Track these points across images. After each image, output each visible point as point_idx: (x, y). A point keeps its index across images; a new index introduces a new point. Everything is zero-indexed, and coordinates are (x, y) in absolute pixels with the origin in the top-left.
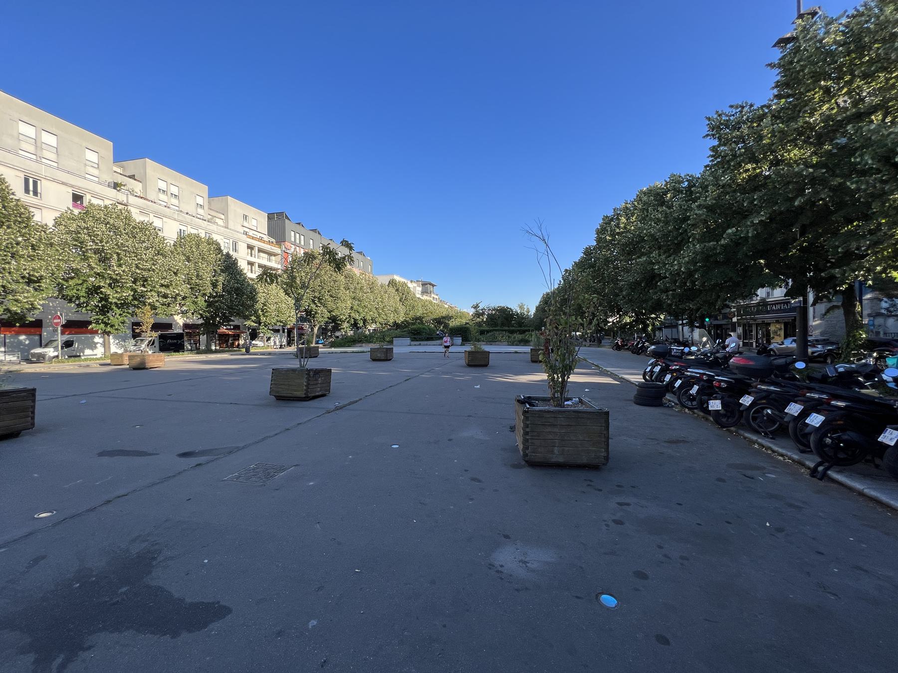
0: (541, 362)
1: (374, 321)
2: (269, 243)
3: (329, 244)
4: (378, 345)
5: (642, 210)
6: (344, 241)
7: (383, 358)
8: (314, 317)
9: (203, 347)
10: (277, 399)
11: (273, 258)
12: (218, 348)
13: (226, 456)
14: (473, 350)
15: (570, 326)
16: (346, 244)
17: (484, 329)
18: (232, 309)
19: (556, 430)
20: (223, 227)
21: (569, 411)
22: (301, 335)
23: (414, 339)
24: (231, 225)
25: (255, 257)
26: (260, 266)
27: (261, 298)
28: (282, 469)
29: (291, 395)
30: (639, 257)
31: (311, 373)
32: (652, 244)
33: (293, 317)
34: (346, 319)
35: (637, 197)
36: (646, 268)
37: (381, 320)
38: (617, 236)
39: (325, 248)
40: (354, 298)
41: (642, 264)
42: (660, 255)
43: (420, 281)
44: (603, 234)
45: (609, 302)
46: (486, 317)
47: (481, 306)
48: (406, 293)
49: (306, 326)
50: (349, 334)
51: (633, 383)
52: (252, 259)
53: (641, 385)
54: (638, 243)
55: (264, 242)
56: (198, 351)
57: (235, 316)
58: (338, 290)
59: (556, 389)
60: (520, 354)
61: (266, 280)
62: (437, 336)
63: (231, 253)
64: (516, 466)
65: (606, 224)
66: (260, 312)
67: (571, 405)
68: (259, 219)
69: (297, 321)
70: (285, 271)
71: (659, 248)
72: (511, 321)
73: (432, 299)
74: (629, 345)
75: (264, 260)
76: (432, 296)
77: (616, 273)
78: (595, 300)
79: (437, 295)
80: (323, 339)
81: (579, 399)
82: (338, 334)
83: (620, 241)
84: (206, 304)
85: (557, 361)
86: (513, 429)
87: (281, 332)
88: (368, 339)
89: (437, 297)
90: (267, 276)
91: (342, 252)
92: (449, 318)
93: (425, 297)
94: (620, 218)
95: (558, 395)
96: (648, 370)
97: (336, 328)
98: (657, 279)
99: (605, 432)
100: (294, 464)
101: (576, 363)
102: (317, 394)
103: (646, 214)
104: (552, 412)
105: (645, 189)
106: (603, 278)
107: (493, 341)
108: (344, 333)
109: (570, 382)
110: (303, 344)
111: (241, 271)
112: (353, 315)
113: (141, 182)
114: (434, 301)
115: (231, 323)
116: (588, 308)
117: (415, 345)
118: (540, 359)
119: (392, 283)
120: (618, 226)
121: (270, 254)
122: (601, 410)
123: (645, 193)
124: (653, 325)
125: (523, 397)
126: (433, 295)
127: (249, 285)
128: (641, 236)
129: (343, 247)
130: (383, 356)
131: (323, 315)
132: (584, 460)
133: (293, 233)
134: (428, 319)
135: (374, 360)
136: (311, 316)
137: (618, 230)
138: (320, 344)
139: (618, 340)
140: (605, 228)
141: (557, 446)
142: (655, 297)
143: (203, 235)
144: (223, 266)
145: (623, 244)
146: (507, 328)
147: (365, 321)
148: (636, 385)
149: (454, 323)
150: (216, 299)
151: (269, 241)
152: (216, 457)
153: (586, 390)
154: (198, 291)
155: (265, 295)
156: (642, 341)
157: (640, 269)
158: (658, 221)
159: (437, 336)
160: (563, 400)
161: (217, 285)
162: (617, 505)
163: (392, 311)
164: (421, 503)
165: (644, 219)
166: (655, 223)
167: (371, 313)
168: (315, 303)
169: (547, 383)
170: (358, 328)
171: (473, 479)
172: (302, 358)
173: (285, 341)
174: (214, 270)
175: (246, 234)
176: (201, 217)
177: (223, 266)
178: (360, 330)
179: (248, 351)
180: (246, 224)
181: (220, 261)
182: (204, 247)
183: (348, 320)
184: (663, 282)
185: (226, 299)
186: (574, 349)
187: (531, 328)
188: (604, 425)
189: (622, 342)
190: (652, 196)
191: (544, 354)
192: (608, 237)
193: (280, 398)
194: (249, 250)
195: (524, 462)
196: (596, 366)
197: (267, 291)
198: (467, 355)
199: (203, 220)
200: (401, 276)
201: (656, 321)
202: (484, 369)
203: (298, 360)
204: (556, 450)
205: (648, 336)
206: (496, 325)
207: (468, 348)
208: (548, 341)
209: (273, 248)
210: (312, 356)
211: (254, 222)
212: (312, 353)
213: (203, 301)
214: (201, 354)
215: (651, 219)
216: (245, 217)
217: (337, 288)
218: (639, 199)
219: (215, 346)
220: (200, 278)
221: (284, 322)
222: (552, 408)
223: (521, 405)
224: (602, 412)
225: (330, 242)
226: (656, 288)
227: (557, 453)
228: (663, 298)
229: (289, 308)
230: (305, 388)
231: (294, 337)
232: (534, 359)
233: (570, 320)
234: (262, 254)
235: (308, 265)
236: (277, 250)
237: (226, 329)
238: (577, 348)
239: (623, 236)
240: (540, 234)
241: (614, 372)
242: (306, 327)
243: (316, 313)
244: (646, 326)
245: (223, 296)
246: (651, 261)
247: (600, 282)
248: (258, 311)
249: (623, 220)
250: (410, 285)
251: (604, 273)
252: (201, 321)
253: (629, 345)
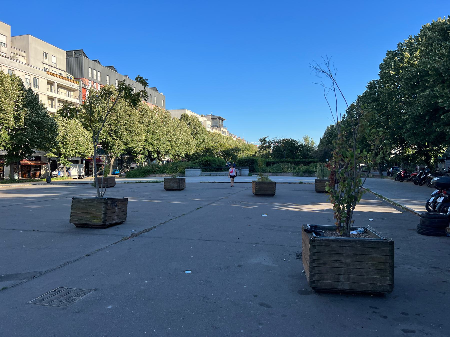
0: (327, 192)
1: (167, 153)
2: (68, 79)
3: (125, 80)
4: (171, 175)
5: (427, 45)
6: (138, 77)
7: (176, 188)
8: (111, 149)
9: (6, 177)
10: (77, 227)
11: (72, 93)
12: (20, 178)
13: (30, 280)
14: (260, 180)
15: (356, 159)
16: (140, 80)
17: (270, 160)
18: (34, 141)
19: (342, 259)
20: (24, 64)
21: (355, 241)
22: (98, 166)
23: (204, 170)
24: (32, 62)
25: (55, 92)
26: (60, 101)
27: (61, 131)
28: (82, 293)
29: (89, 223)
30: (423, 91)
31: (109, 203)
32: (436, 78)
33: (91, 149)
34: (141, 151)
35: (421, 32)
36: (430, 102)
37: (173, 152)
38: (400, 71)
39: (121, 84)
40: (148, 132)
41: (425, 98)
42: (444, 89)
43: (210, 116)
44: (387, 69)
45: (393, 135)
46: (272, 149)
47: (267, 140)
48: (197, 127)
49: (104, 157)
50: (144, 165)
51: (416, 213)
52: (52, 95)
53: (424, 216)
54: (422, 76)
55: (63, 78)
56: (2, 181)
57: (37, 148)
58: (132, 123)
59: (342, 220)
60: (305, 185)
61: (67, 115)
62: (226, 167)
63: (33, 88)
64: (303, 293)
65: (390, 59)
66: (60, 144)
67: (356, 235)
68: (57, 56)
69: (95, 153)
70: (84, 106)
71: (443, 82)
72: (296, 153)
73: (221, 132)
74: (412, 176)
75: (63, 95)
76: (221, 129)
77: (399, 106)
78: (381, 133)
79: (226, 129)
80: (119, 169)
81: (364, 228)
82: (133, 165)
83: (404, 75)
84: (9, 137)
85: (343, 192)
86: (299, 256)
87: (80, 163)
88: (161, 170)
89: (226, 131)
90: (68, 111)
91: (137, 88)
92: (237, 150)
93: (215, 131)
94: (404, 53)
95: (343, 225)
96: (431, 201)
97: (132, 159)
98: (441, 112)
99: (390, 261)
100: (94, 289)
101: (361, 194)
102: (114, 222)
103: (430, 48)
104: (338, 241)
105: (429, 24)
106: (387, 111)
107: (279, 172)
108: (138, 164)
109: (355, 211)
110: (100, 174)
111: (42, 106)
112: (147, 147)
113: (25, 52)
114: (223, 135)
115: (33, 155)
116: (374, 141)
117: (206, 176)
118: (326, 190)
119: (184, 117)
120: (401, 61)
121: (69, 90)
122: (385, 239)
123: (429, 29)
124: (436, 157)
125: (309, 227)
126: (222, 129)
127: (49, 119)
128: (425, 70)
129: (138, 83)
130: (175, 186)
131: (120, 147)
132: (370, 287)
133: (90, 70)
134: (218, 150)
135: (168, 190)
136: (107, 148)
137: (401, 65)
138: (116, 174)
139: (401, 171)
140: (389, 63)
141: (343, 273)
142: (438, 130)
143: (6, 72)
144: (25, 101)
145: (407, 79)
146: (292, 160)
147: (158, 153)
148: (419, 215)
149: (242, 155)
150: (18, 132)
151: (68, 77)
152: (20, 281)
153: (370, 220)
154: (2, 124)
155: (64, 128)
156: (425, 172)
157: (423, 102)
158: (442, 56)
159: (226, 167)
160: (349, 229)
161: (19, 119)
162: (403, 333)
163: (184, 144)
164: (213, 327)
165: (428, 53)
166: (439, 58)
167: (165, 146)
168: (112, 136)
169: (333, 213)
170: (152, 160)
171: (262, 304)
172: (100, 187)
173: (83, 171)
174: (17, 105)
175: (46, 71)
176: (5, 55)
177: (25, 101)
178: (154, 162)
179: (49, 181)
180: (46, 61)
181: (22, 96)
182: (8, 83)
183: (142, 152)
184: (447, 116)
185: (28, 132)
186: (360, 180)
187: (315, 160)
188: (389, 255)
189: (404, 173)
190: (436, 31)
191: (330, 185)
192: (391, 72)
193: (79, 226)
194: (49, 86)
195: (311, 289)
196: (379, 196)
197: (66, 125)
198: (254, 185)
199: (6, 57)
200: (192, 111)
201: (438, 153)
202: (270, 199)
203: (96, 189)
204: (342, 278)
205: (430, 167)
206: (282, 157)
207: (255, 178)
208: (333, 173)
209: (72, 84)
210: (109, 186)
211: (54, 60)
212: (110, 183)
213: (6, 134)
214: (5, 183)
215: (435, 54)
216: (45, 55)
217: (131, 122)
218: (423, 34)
219: (18, 176)
220: (4, 112)
221: (82, 153)
222: (338, 238)
223: (308, 234)
224: (386, 242)
225: (125, 78)
226: (439, 121)
227: (343, 281)
228: (446, 130)
229: (87, 141)
230: (103, 216)
231: (92, 168)
232: (319, 189)
233: (356, 153)
234: (61, 90)
235: (105, 100)
236: (75, 86)
237: (28, 160)
238: (363, 179)
239: (407, 71)
240: (326, 70)
241: (396, 202)
242: (103, 159)
243: (113, 145)
244: (429, 158)
245: (25, 129)
246: (435, 95)
247: (383, 115)
248: (58, 143)
249: (407, 55)
250: (200, 119)
251: (388, 107)
252: (5, 153)
253: (412, 176)
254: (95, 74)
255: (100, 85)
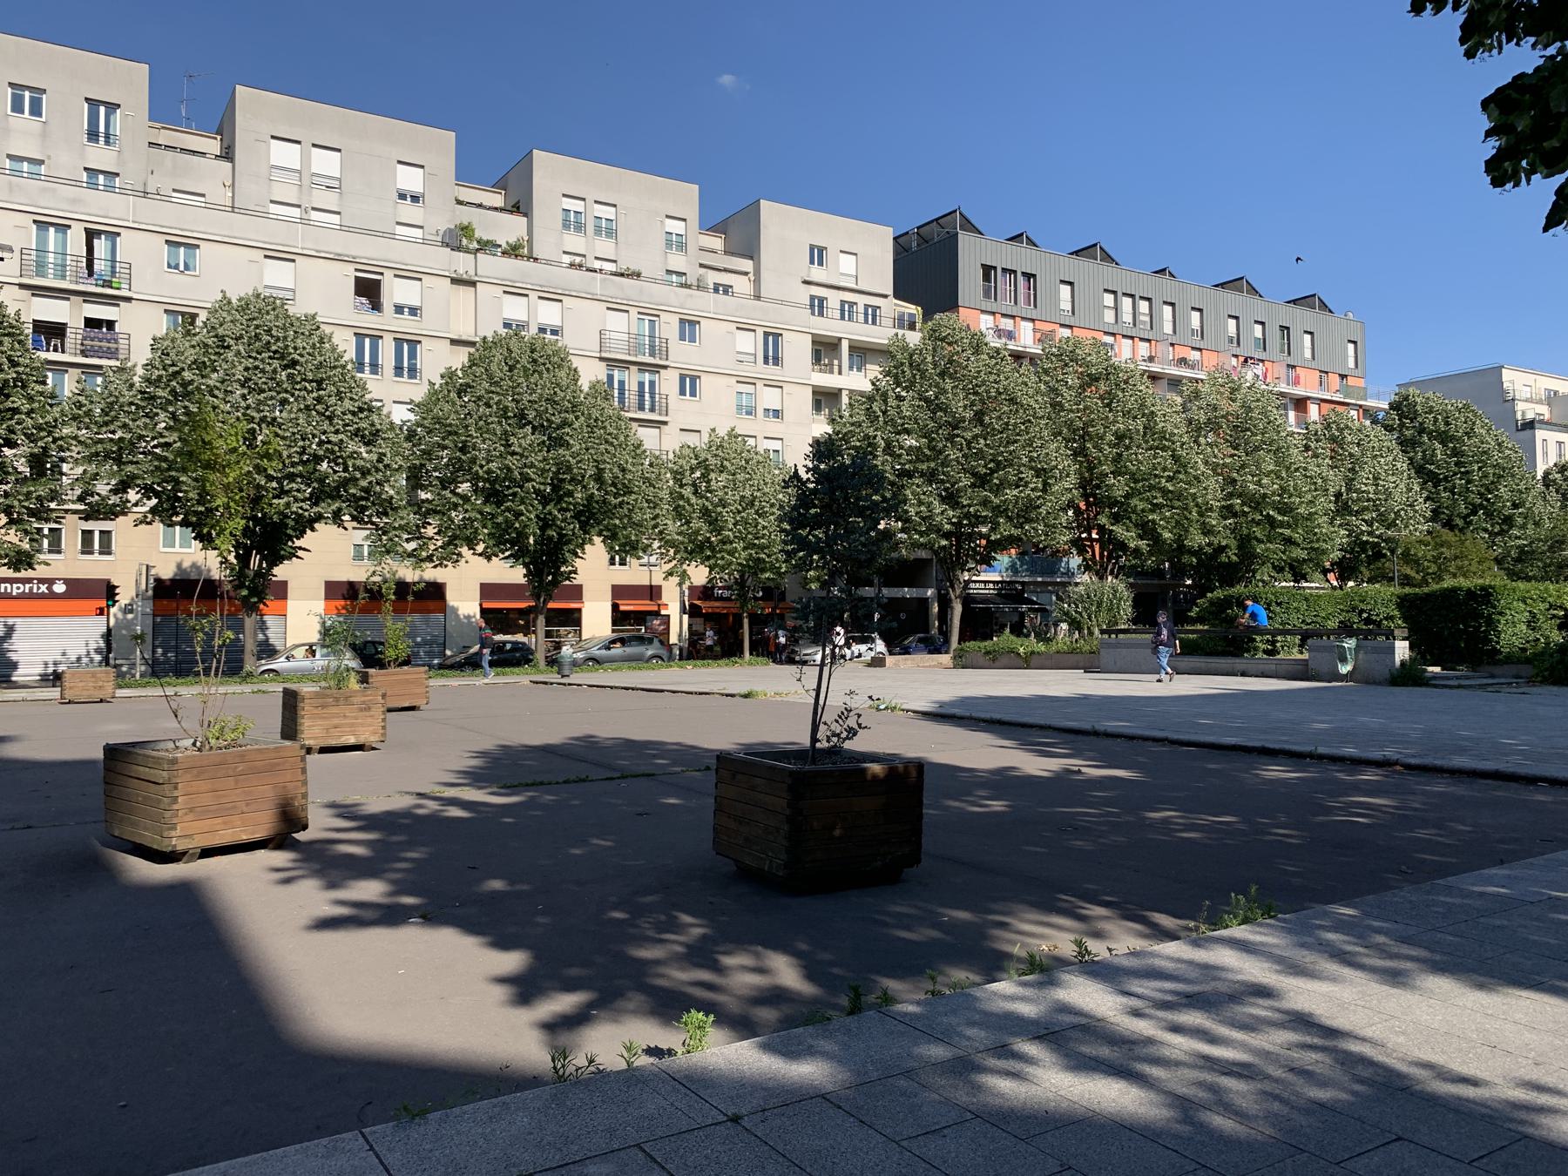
180: (817, 273)
211: (847, 264)
254: (1170, 318)
255: (1033, 320)
